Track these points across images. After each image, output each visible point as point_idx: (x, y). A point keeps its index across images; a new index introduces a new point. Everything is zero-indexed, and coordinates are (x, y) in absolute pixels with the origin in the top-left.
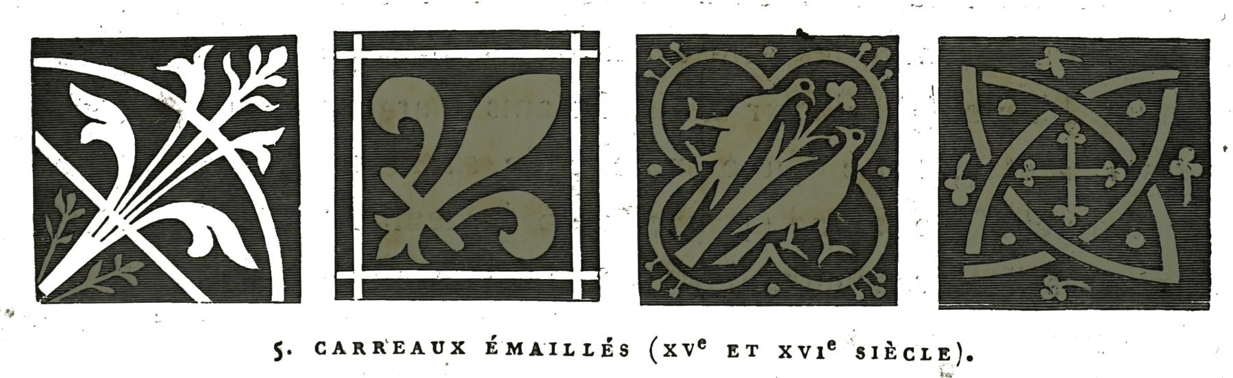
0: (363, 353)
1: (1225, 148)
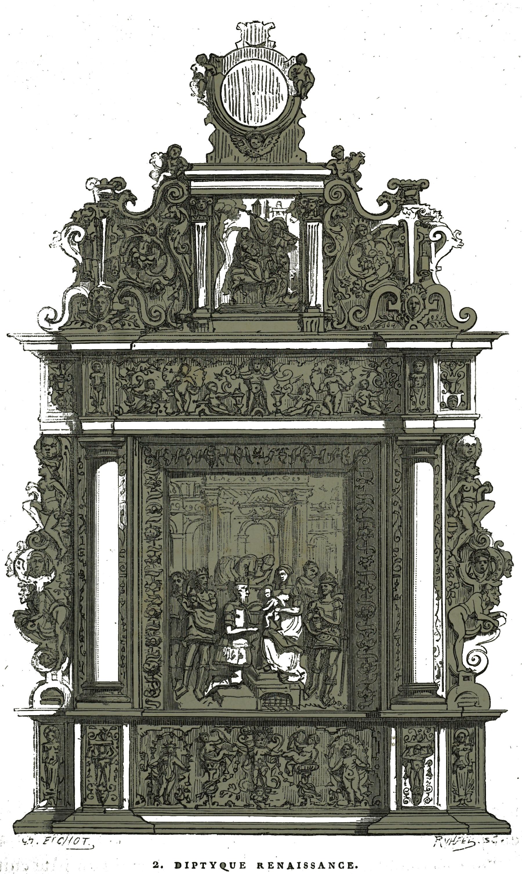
0: (262, 868)
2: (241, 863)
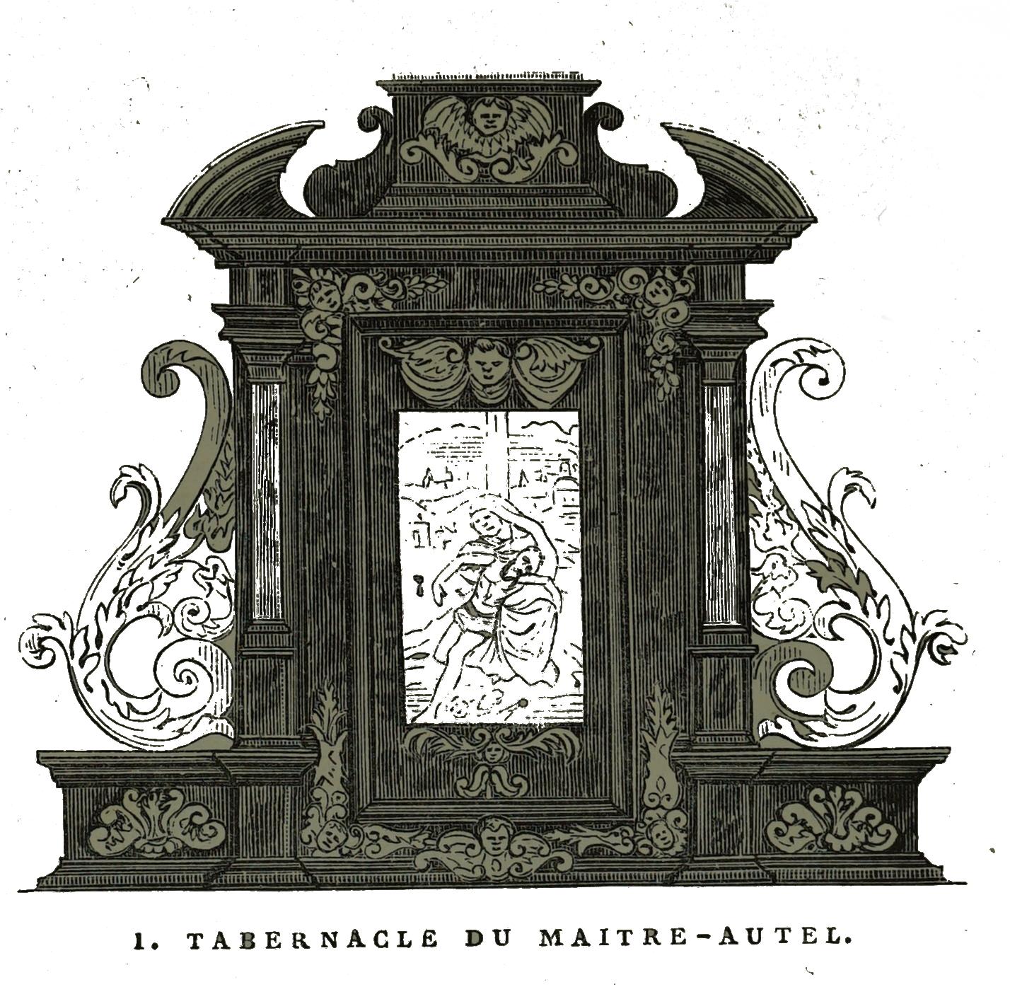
0: (305, 946)
1: (993, 850)
2: (674, 930)
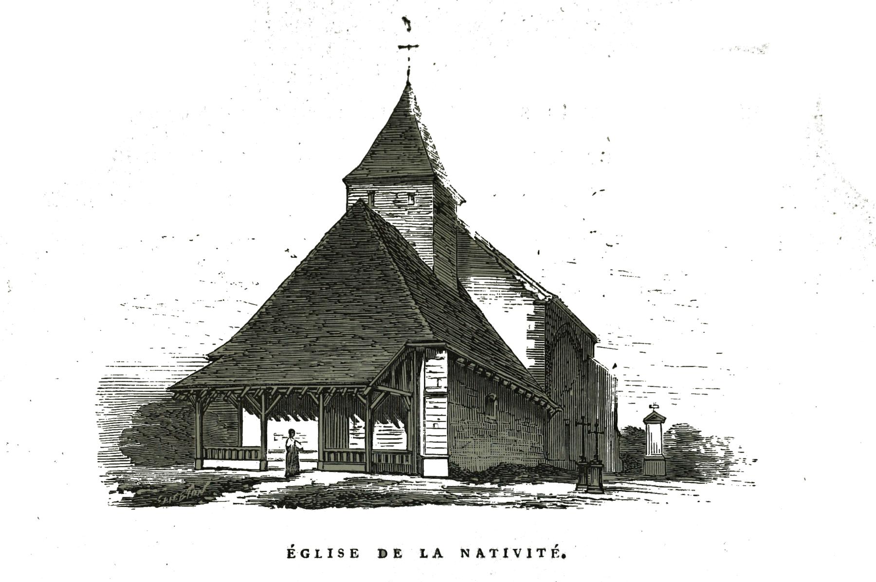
2: (352, 550)
